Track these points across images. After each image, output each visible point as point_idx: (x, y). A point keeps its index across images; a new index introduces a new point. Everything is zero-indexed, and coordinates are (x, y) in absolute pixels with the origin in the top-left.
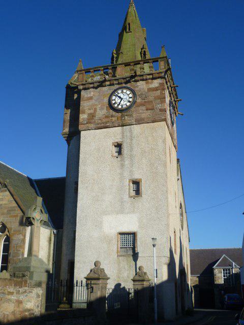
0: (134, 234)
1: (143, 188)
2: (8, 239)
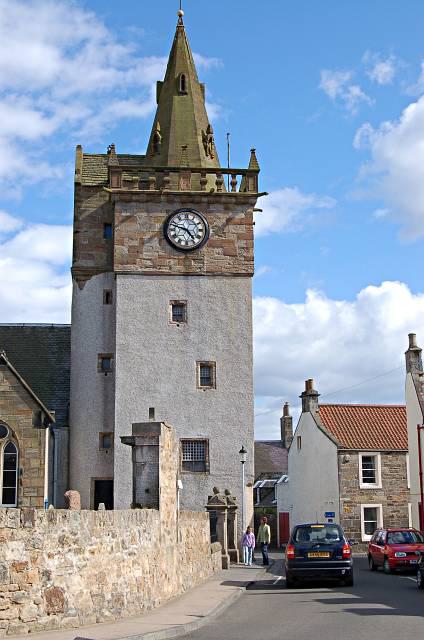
0: (205, 443)
1: (219, 375)
2: (10, 448)
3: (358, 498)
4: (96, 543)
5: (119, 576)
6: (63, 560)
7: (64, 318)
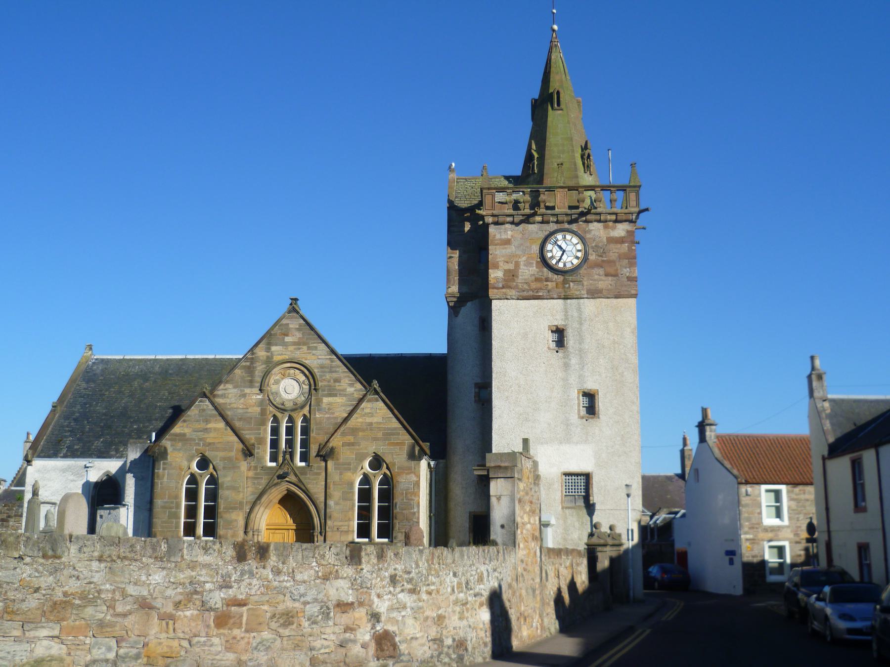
1: (601, 404)
3: (761, 535)
4: (433, 584)
5: (461, 619)
6: (395, 601)
7: (438, 346)
